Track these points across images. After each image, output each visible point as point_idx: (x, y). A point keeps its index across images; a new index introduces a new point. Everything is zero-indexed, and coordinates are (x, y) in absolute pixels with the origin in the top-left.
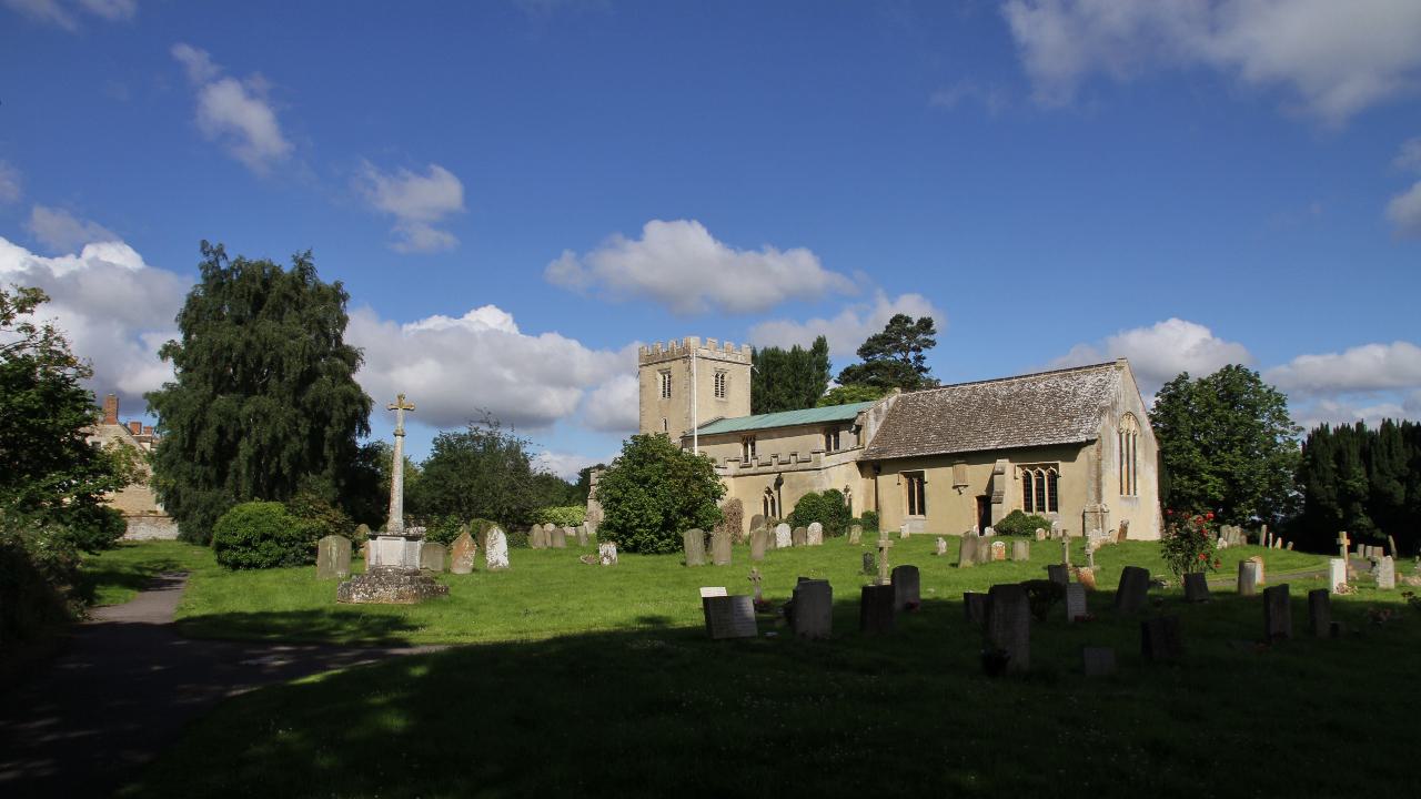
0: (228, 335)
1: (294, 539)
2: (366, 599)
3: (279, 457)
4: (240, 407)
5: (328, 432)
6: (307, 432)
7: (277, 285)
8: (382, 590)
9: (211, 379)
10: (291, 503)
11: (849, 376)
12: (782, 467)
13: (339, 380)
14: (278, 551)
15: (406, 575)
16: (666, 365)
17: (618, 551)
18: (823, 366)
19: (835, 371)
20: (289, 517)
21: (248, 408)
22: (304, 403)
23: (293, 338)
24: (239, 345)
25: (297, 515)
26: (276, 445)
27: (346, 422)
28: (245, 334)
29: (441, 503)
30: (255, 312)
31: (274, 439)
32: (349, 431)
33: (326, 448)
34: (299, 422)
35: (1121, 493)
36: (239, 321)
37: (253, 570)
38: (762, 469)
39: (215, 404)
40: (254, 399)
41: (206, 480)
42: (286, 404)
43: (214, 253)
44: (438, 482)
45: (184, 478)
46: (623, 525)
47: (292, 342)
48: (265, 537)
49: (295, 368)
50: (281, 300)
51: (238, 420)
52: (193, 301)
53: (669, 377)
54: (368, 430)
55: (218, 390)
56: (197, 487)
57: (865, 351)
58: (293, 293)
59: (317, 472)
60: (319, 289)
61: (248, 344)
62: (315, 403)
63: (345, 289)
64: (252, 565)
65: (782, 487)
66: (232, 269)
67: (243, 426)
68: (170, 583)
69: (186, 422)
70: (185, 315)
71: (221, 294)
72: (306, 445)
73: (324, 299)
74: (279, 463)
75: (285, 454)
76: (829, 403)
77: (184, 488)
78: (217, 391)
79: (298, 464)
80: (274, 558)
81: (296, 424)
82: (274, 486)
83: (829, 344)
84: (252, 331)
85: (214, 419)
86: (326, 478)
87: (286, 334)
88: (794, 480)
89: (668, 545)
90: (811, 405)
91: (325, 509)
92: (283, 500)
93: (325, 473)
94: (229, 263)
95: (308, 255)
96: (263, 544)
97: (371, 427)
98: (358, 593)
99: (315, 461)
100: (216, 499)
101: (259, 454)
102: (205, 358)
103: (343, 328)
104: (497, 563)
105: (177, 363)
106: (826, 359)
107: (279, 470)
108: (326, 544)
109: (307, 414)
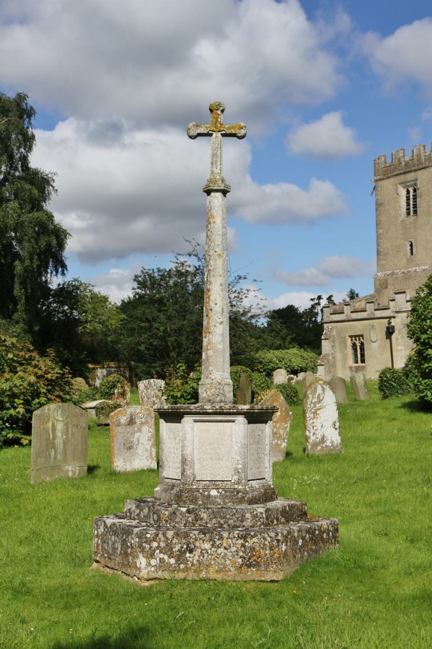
8: (207, 546)
15: (253, 501)
16: (410, 177)
29: (147, 349)
35: (362, 344)
38: (355, 316)
44: (143, 325)
53: (415, 190)
54: (64, 266)
63: (31, 102)
65: (394, 337)
91: (31, 359)
97: (67, 263)
103: (30, 149)
104: (323, 440)
108: (45, 419)
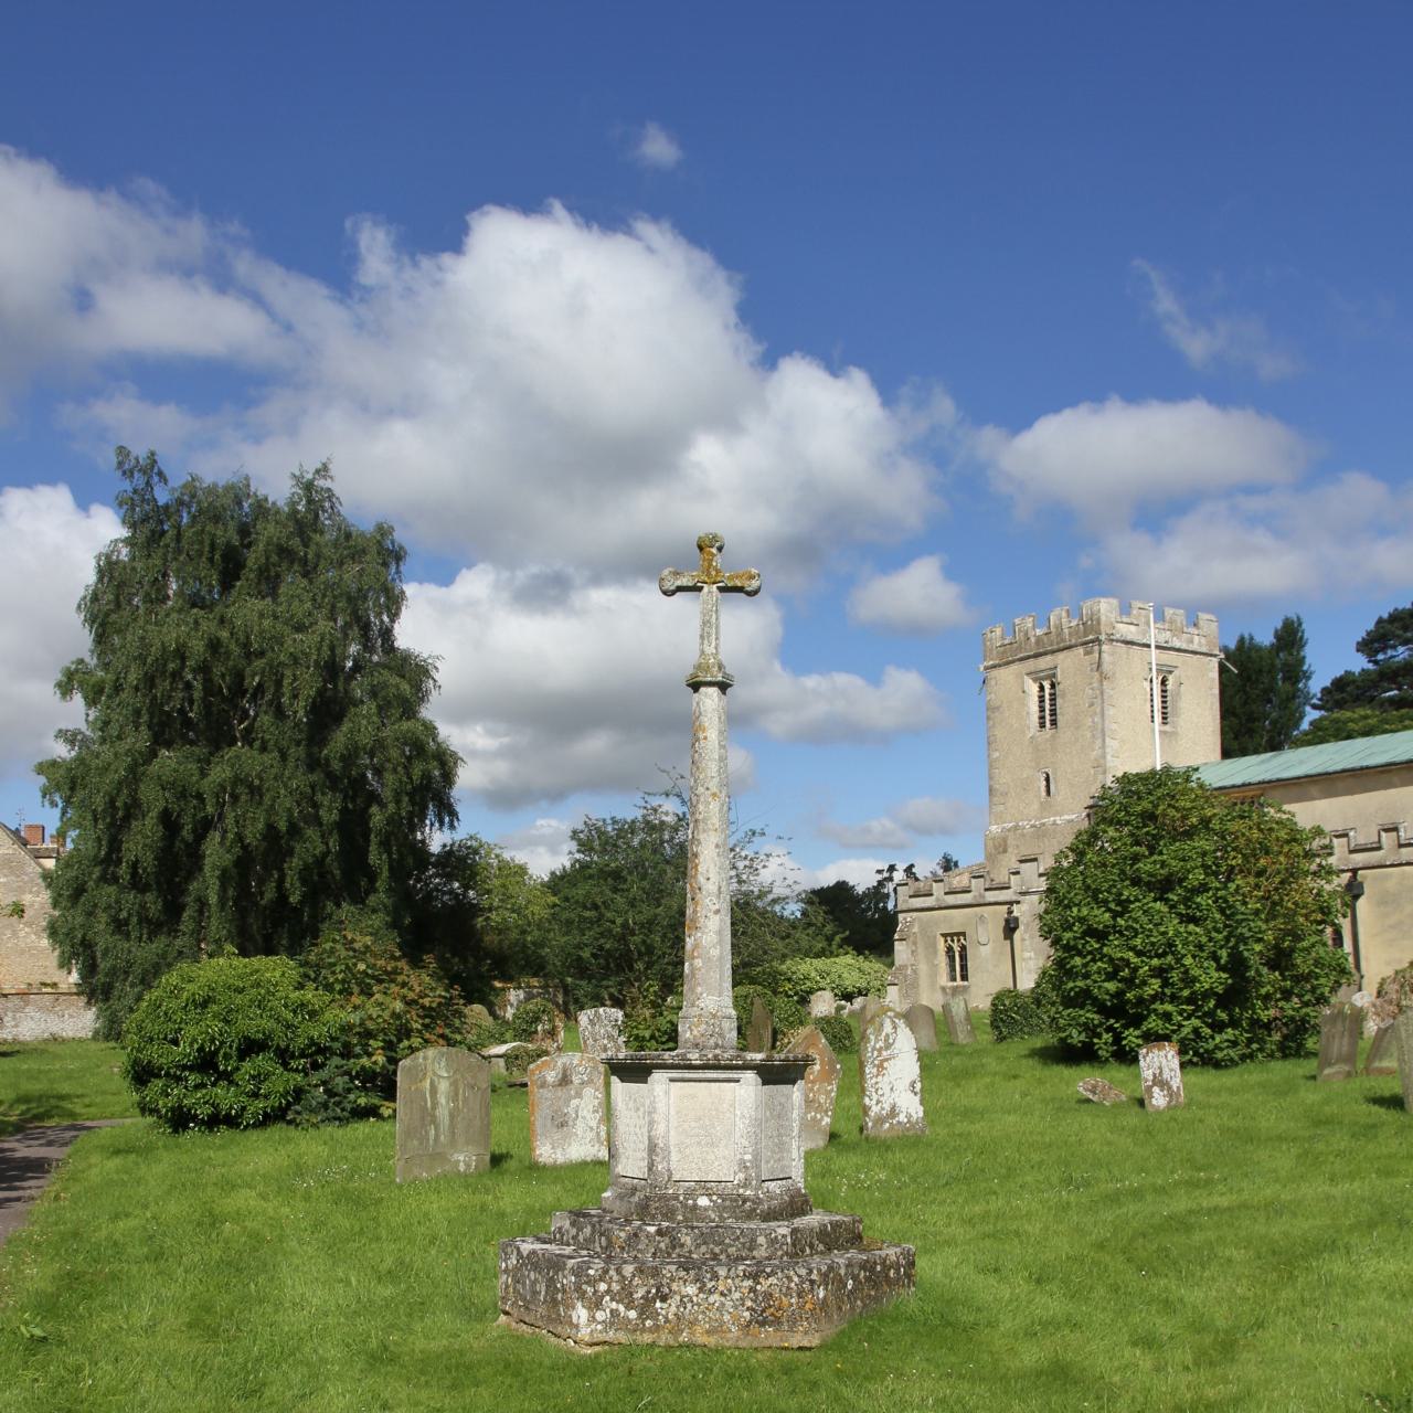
0: (175, 629)
1: (322, 1050)
2: (624, 1324)
3: (281, 870)
4: (203, 774)
5: (377, 817)
6: (335, 816)
7: (267, 532)
8: (691, 1290)
9: (145, 718)
10: (312, 957)
11: (1343, 692)
12: (1360, 859)
13: (396, 712)
14: (281, 1081)
16: (1044, 663)
17: (1183, 1065)
18: (1296, 673)
19: (1317, 684)
20: (309, 995)
21: (220, 773)
22: (327, 760)
23: (300, 628)
24: (198, 647)
25: (329, 987)
26: (277, 844)
27: (411, 795)
28: (209, 626)
29: (594, 955)
30: (226, 586)
31: (271, 832)
32: (416, 819)
33: (373, 848)
34: (318, 797)
35: (963, 948)
36: (195, 602)
37: (224, 1133)
38: (951, 900)
39: (154, 767)
40: (229, 753)
41: (144, 920)
42: (291, 763)
43: (143, 471)
44: (587, 914)
45: (104, 917)
46: (1120, 994)
47: (299, 636)
48: (250, 1048)
49: (305, 686)
50: (274, 558)
51: (200, 797)
52: (108, 569)
53: (1053, 686)
54: (453, 814)
55: (161, 739)
56: (127, 936)
57: (1370, 645)
58: (296, 542)
59: (359, 899)
60: (348, 536)
61: (214, 646)
62: (349, 758)
64: (216, 1121)
66: (180, 502)
67: (210, 809)
68: (89, 1128)
69: (99, 802)
70: (95, 598)
71: (161, 552)
72: (334, 844)
73: (357, 554)
74: (281, 881)
75: (294, 864)
76: (1319, 735)
77: (103, 938)
78: (161, 739)
79: (320, 887)
80: (274, 1101)
81: (316, 806)
82: (273, 926)
83: (1309, 631)
84: (222, 621)
85: (154, 799)
86: (374, 911)
87: (281, 623)
88: (1391, 885)
89: (1234, 1044)
90: (1275, 746)
91: (395, 972)
92: (292, 954)
93: (372, 900)
94: (174, 489)
95: (323, 471)
96: (247, 1065)
97: (458, 808)
98: (596, 1304)
99: (353, 881)
100: (164, 956)
101: (244, 863)
102: (133, 677)
103: (394, 616)
104: (893, 1112)
105: (91, 702)
106: (1302, 661)
107: (282, 897)
108: (418, 1074)
109: (333, 781)
